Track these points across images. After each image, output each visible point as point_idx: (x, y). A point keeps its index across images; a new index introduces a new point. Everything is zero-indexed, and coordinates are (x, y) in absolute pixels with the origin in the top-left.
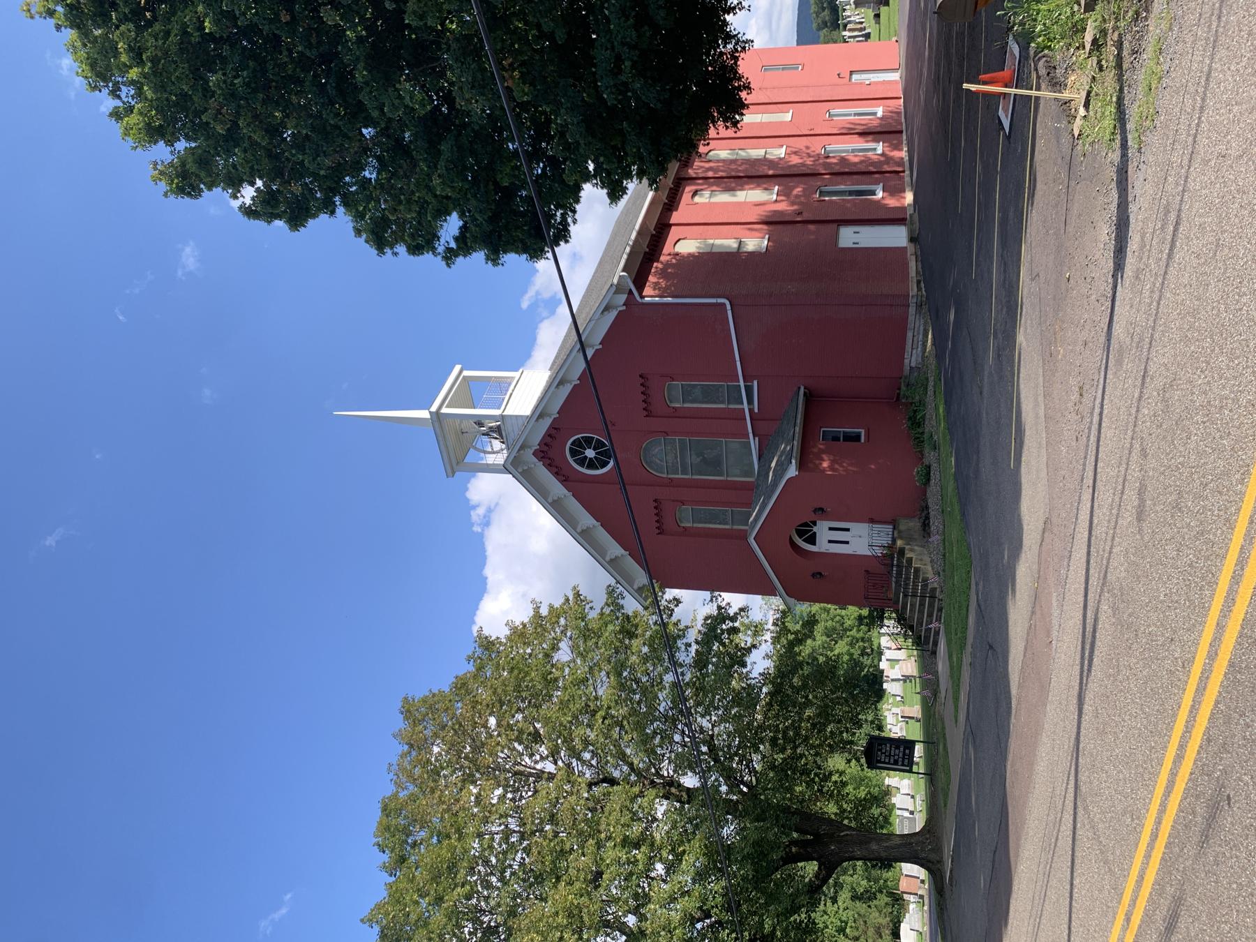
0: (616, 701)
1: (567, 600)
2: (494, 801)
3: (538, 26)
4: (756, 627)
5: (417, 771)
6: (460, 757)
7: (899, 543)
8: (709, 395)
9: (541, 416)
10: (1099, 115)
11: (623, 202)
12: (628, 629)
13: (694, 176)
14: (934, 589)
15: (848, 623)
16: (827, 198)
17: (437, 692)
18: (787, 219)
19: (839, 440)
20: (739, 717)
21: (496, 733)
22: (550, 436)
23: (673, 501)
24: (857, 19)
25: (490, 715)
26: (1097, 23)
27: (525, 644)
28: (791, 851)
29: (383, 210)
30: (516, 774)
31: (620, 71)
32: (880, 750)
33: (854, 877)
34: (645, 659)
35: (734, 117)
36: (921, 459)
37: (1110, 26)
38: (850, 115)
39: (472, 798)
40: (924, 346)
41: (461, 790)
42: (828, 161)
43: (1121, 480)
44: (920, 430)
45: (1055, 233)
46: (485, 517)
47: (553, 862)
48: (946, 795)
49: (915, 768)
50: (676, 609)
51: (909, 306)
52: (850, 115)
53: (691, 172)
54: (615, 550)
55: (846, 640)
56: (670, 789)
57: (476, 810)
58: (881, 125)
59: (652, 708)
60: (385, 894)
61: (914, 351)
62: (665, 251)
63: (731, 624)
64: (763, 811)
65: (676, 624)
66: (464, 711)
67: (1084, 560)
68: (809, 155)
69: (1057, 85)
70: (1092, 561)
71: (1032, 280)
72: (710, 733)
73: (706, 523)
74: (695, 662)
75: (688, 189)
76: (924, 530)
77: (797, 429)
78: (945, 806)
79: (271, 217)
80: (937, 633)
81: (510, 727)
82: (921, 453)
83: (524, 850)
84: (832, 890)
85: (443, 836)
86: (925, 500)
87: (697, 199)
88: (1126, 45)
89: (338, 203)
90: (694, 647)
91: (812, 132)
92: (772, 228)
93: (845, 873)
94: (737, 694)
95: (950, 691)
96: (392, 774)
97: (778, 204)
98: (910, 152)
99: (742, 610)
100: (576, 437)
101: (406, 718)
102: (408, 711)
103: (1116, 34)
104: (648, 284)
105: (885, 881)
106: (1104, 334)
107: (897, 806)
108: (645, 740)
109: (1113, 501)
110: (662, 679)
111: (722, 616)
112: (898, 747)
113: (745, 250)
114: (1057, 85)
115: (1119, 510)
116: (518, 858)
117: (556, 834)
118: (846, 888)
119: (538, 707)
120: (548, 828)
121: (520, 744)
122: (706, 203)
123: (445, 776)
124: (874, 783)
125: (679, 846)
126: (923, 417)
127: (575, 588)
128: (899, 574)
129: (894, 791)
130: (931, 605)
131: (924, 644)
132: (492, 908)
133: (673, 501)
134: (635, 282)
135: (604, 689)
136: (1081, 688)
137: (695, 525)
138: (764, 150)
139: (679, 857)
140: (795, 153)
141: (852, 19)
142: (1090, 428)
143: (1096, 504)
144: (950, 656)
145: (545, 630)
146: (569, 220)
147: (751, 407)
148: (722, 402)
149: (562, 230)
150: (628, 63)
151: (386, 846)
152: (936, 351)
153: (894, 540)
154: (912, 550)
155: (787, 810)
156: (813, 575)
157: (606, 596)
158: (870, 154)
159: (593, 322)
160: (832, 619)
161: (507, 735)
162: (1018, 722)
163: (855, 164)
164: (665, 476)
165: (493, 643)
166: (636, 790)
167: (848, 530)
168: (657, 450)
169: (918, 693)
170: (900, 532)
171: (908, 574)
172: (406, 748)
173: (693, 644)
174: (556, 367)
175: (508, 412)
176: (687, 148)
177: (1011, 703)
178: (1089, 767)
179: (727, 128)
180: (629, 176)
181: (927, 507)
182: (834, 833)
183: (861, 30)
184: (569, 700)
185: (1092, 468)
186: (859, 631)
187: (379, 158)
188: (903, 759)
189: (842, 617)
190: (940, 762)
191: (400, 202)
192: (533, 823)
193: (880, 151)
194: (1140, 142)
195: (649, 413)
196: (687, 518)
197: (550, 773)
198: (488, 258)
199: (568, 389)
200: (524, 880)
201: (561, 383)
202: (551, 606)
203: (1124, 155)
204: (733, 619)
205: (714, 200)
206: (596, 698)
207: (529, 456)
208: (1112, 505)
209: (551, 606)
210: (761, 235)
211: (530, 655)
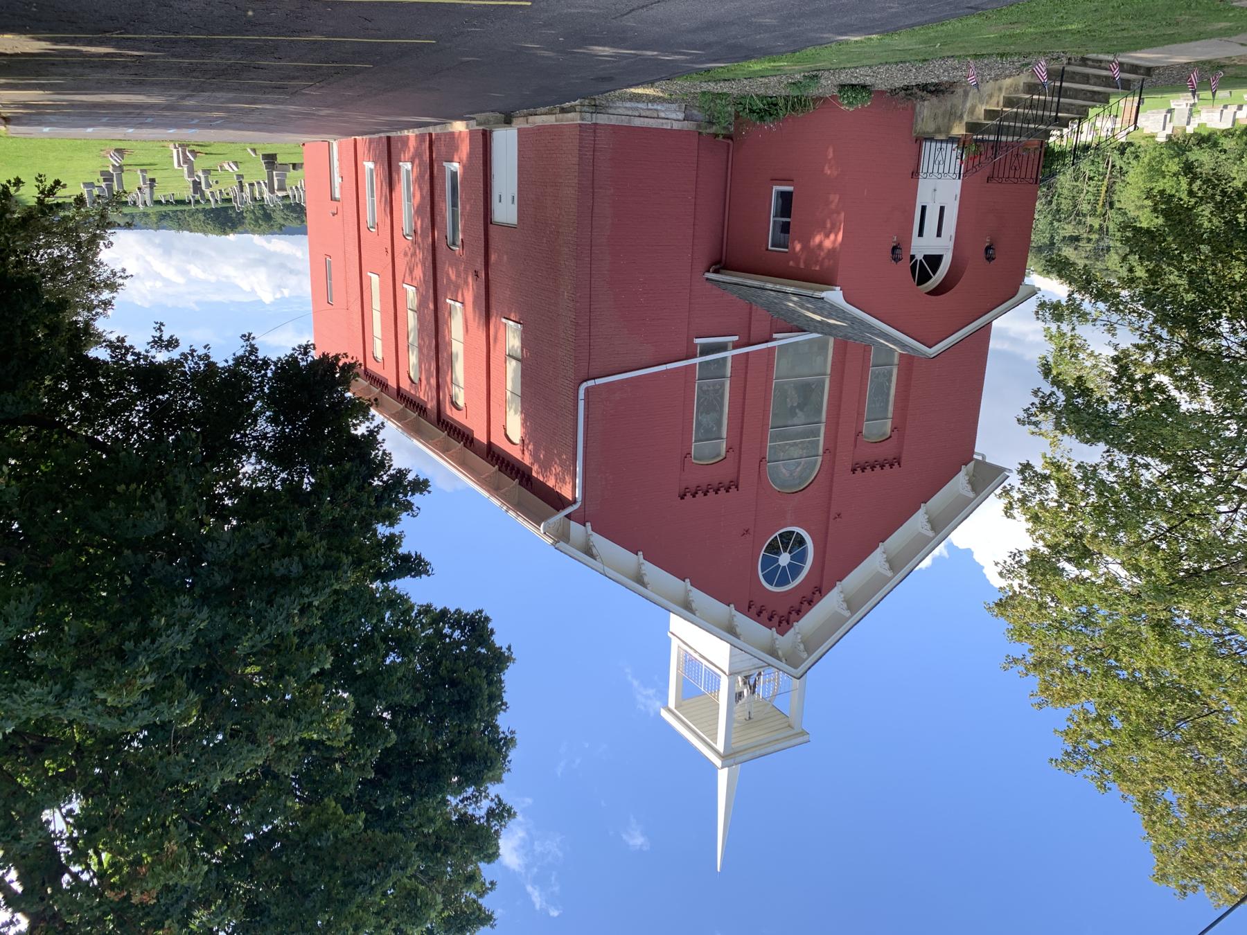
8: (711, 405)
13: (435, 402)
14: (1051, 74)
18: (483, 293)
19: (789, 223)
23: (855, 446)
40: (655, 100)
51: (596, 124)
53: (431, 405)
61: (662, 115)
68: (414, 254)
75: (449, 412)
76: (943, 92)
77: (769, 286)
86: (894, 92)
87: (461, 403)
92: (493, 312)
97: (466, 302)
100: (762, 552)
113: (519, 351)
126: (762, 98)
130: (1073, 77)
133: (855, 446)
137: (890, 415)
140: (411, 272)
147: (730, 345)
148: (723, 385)
153: (952, 140)
156: (990, 259)
163: (422, 197)
164: (820, 459)
167: (924, 208)
168: (784, 471)
169: (1214, 94)
170: (938, 131)
181: (907, 88)
193: (408, 166)
196: (878, 426)
205: (462, 384)
207: (785, 642)
210: (502, 327)
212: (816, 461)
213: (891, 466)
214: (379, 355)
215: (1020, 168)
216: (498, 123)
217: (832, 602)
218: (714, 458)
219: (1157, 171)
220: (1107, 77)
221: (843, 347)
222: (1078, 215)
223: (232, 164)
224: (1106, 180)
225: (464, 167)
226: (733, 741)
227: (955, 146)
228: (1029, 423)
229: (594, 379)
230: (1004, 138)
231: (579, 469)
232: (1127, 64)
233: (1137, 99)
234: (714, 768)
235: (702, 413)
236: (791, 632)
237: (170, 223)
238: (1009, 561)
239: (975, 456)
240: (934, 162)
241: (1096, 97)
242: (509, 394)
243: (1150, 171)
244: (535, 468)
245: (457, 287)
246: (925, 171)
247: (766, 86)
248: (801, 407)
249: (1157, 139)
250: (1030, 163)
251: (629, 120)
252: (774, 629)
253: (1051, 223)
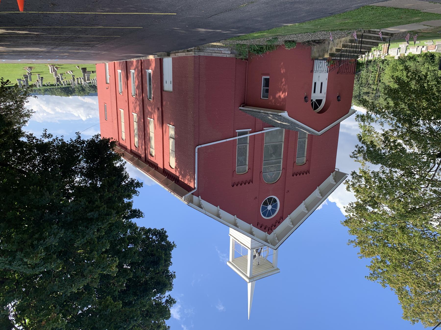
8: (242, 153)
16: (152, 96)
23: (293, 167)
40: (220, 47)
42: (138, 94)
44: (265, 47)
53: (143, 156)
61: (223, 52)
62: (174, 172)
68: (136, 102)
73: (304, 150)
75: (149, 158)
76: (321, 43)
86: (304, 43)
87: (153, 154)
91: (127, 101)
99: (360, 140)
100: (262, 205)
122: (155, 151)
126: (258, 46)
130: (366, 37)
133: (293, 167)
137: (305, 156)
138: (134, 122)
140: (135, 109)
148: (246, 146)
152: (222, 40)
153: (324, 59)
154: (331, 49)
156: (339, 100)
163: (139, 82)
164: (281, 172)
167: (315, 83)
168: (269, 176)
169: (415, 43)
170: (320, 56)
175: (249, 245)
180: (129, 205)
181: (308, 42)
196: (301, 160)
207: (270, 237)
210: (168, 127)
212: (280, 172)
213: (306, 173)
214: (124, 138)
215: (349, 68)
217: (287, 222)
218: (244, 172)
219: (395, 69)
220: (377, 37)
221: (288, 132)
222: (368, 84)
223: (70, 72)
224: (378, 72)
225: (153, 71)
226: (253, 273)
227: (326, 61)
228: (354, 157)
229: (201, 145)
230: (342, 59)
232: (384, 32)
233: (388, 44)
235: (239, 157)
237: (49, 93)
238: (349, 206)
239: (336, 170)
240: (319, 67)
241: (374, 44)
242: (170, 151)
243: (393, 69)
244: (180, 177)
245: (151, 113)
246: (315, 70)
247: (259, 41)
249: (395, 58)
250: (352, 67)
251: (212, 54)
252: (266, 232)
253: (359, 88)
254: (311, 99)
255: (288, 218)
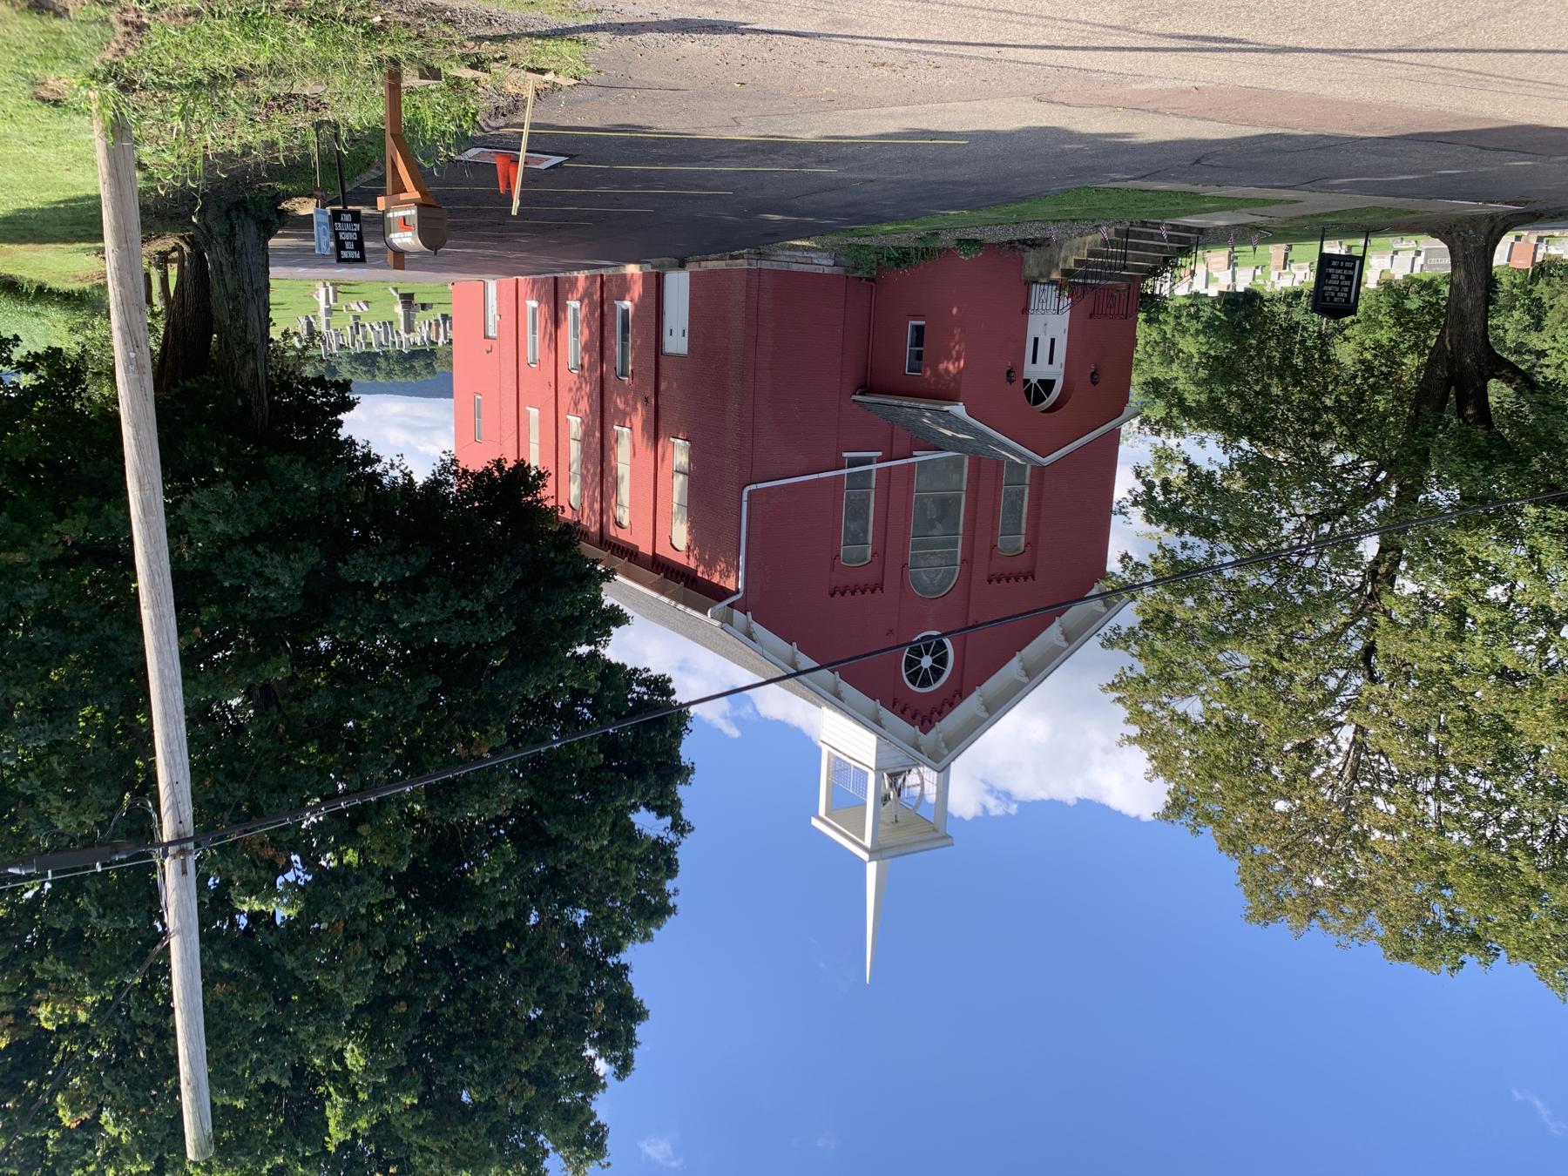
0: (1259, 643)
1: (1119, 699)
2: (1393, 809)
3: (422, 708)
4: (1160, 457)
5: (1348, 909)
6: (1330, 851)
7: (1055, 276)
8: (858, 513)
9: (878, 722)
10: (555, 58)
11: (627, 610)
12: (1163, 622)
14: (1117, 232)
15: (1155, 336)
17: (1240, 877)
18: (652, 416)
20: (1281, 483)
21: (1298, 802)
22: (903, 711)
23: (991, 559)
24: (425, 329)
25: (1272, 808)
26: (454, 64)
27: (1177, 758)
28: (1472, 416)
29: (623, 903)
30: (1355, 778)
31: (473, 614)
32: (1332, 298)
33: (1509, 328)
34: (1202, 601)
35: (533, 477)
36: (948, 250)
37: (457, 51)
38: (534, 339)
39: (1389, 837)
41: (1375, 852)
43: (994, 15)
44: (913, 253)
45: (686, 102)
46: (998, 798)
47: (1484, 734)
48: (1399, 212)
49: (1358, 252)
50: (1136, 560)
52: (534, 339)
53: (594, 529)
54: (1053, 634)
55: (1178, 338)
56: (1381, 575)
57: (1405, 834)
58: (547, 303)
59: (1268, 595)
60: (1524, 965)
63: (1157, 489)
64: (1415, 452)
65: (1156, 560)
66: (1267, 842)
67: (1092, 54)
68: (580, 388)
69: (517, 104)
70: (1095, 45)
71: (739, 125)
72: (1304, 519)
74: (1207, 537)
75: (613, 533)
76: (1040, 245)
77: (905, 404)
78: (1412, 213)
79: (630, 1040)
80: (1175, 227)
81: (1291, 782)
82: (940, 251)
83: (1464, 771)
84: (1526, 357)
85: (1442, 881)
86: (1001, 245)
87: (625, 523)
88: (480, 32)
89: (616, 961)
90: (1187, 537)
92: (662, 434)
93: (1502, 340)
94: (1252, 483)
95: (1254, 210)
96: (1351, 944)
98: (579, 268)
99: (1138, 475)
100: (904, 674)
101: (1274, 919)
102: (1264, 916)
103: (466, 43)
104: (722, 584)
105: (1515, 286)
106: (811, 41)
107: (1408, 272)
108: (1311, 605)
109: (1018, 23)
110: (1230, 580)
111: (1147, 501)
112: (1329, 276)
113: (686, 466)
114: (517, 104)
115: (1032, 15)
116: (1476, 781)
117: (1442, 729)
118: (1523, 338)
119: (1263, 745)
120: (1432, 739)
121: (1314, 770)
123: (1356, 873)
124: (1373, 302)
125: (1465, 565)
126: (897, 249)
127: (1104, 690)
128: (1096, 276)
129: (1385, 276)
130: (1139, 235)
131: (1188, 243)
132: (1548, 820)
133: (991, 559)
134: (720, 600)
135: (1241, 657)
136: (1263, 50)
137: (1023, 531)
139: (1480, 565)
140: (576, 404)
141: (425, 335)
142: (926, 53)
143: (1023, 43)
144: (1207, 211)
145: (1160, 730)
146: (644, 675)
148: (868, 495)
149: (656, 685)
150: (464, 603)
151: (1456, 958)
153: (1052, 282)
154: (1065, 261)
155: (1414, 421)
156: (1095, 383)
157: (1116, 649)
158: (580, 316)
159: (766, 653)
160: (1150, 356)
161: (1301, 788)
162: (1301, 126)
163: (591, 333)
164: (958, 569)
165: (1175, 800)
166: (1382, 620)
167: (1036, 340)
170: (1041, 275)
171: (1096, 265)
172: (1315, 922)
173: (1183, 539)
174: (817, 699)
176: (571, 533)
177: (1275, 135)
178: (1371, 36)
179: (544, 485)
180: (597, 601)
181: (1011, 242)
182: (1448, 359)
183: (438, 325)
184: (1256, 705)
185: (975, 48)
186: (1166, 322)
187: (563, 905)
188: (1344, 268)
189: (1147, 343)
190: (1351, 220)
191: (617, 882)
192: (1425, 759)
193: (577, 304)
194: (591, 11)
195: (878, 587)
197: (1355, 732)
198: (686, 782)
199: (845, 688)
200: (1507, 775)
201: (837, 695)
202: (1128, 721)
203: (603, 28)
204: (1150, 486)
206: (1254, 668)
207: (928, 739)
208: (1025, 24)
209: (1128, 721)
210: (670, 449)
211: (1192, 751)
216: (672, 267)
217: (971, 705)
221: (976, 464)
223: (362, 304)
225: (635, 305)
231: (742, 563)
234: (863, 864)
236: (933, 731)
242: (675, 506)
245: (625, 414)
247: (899, 240)
248: (940, 519)
254: (1025, 377)
255: (974, 695)
